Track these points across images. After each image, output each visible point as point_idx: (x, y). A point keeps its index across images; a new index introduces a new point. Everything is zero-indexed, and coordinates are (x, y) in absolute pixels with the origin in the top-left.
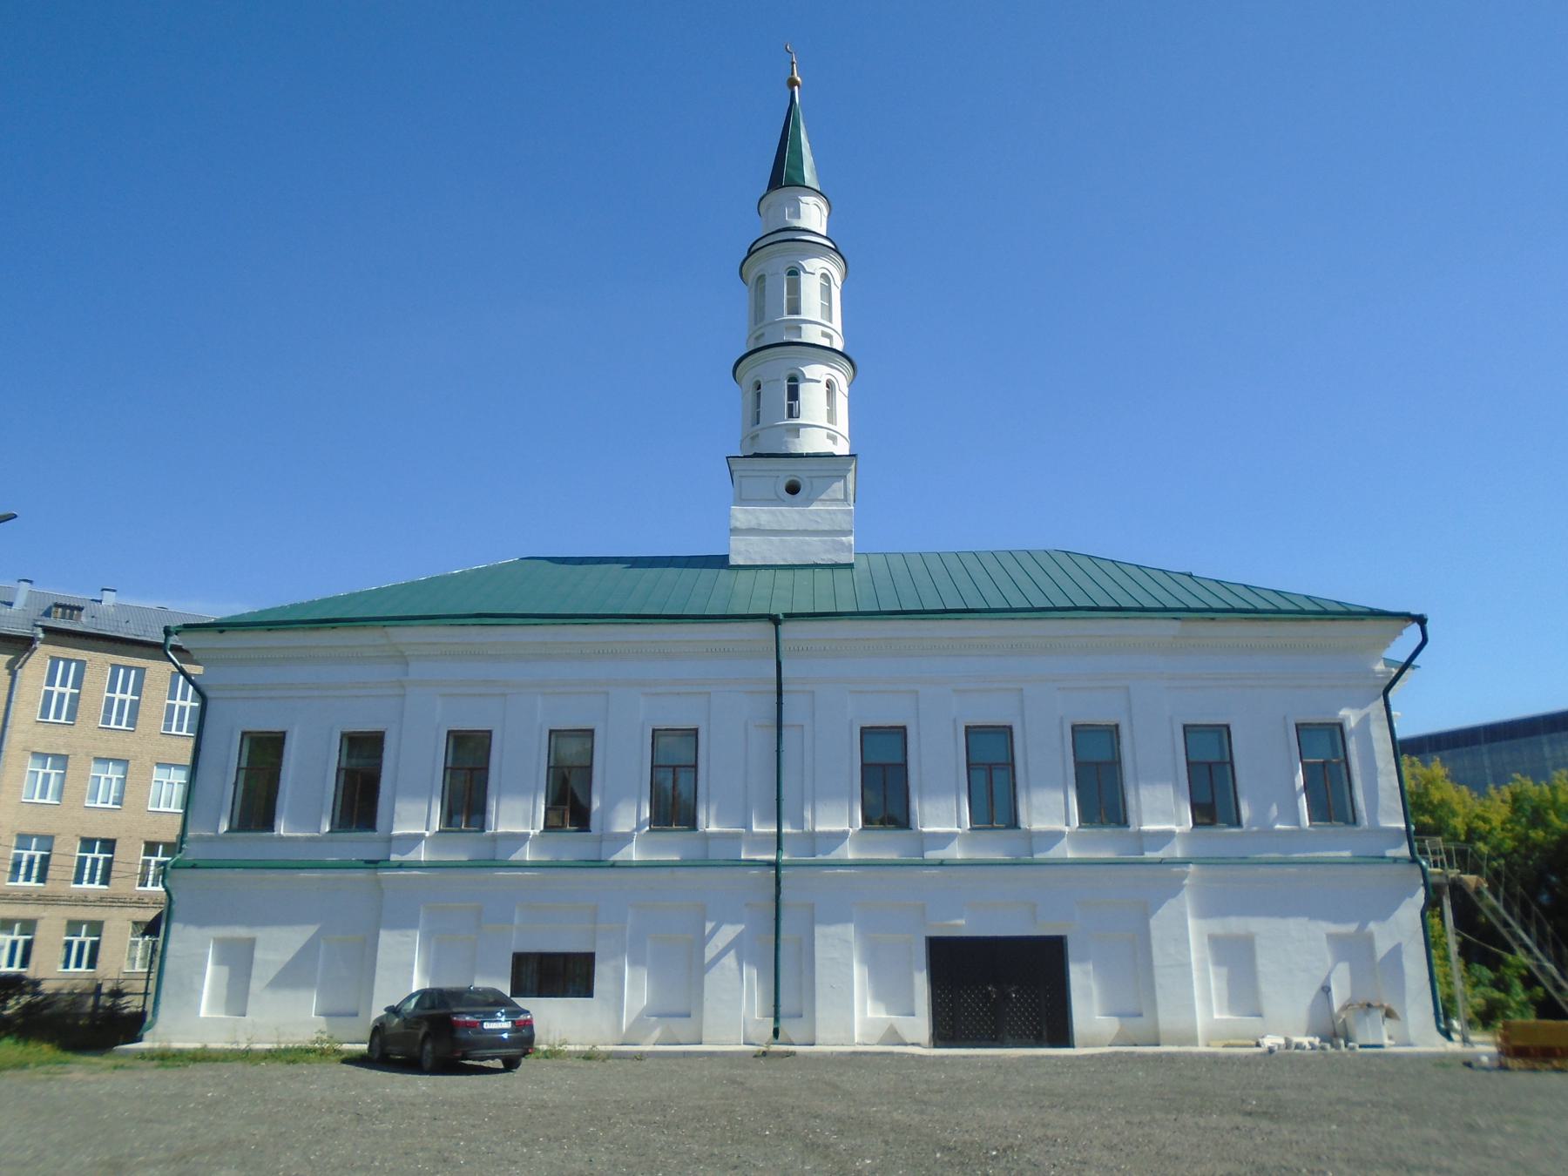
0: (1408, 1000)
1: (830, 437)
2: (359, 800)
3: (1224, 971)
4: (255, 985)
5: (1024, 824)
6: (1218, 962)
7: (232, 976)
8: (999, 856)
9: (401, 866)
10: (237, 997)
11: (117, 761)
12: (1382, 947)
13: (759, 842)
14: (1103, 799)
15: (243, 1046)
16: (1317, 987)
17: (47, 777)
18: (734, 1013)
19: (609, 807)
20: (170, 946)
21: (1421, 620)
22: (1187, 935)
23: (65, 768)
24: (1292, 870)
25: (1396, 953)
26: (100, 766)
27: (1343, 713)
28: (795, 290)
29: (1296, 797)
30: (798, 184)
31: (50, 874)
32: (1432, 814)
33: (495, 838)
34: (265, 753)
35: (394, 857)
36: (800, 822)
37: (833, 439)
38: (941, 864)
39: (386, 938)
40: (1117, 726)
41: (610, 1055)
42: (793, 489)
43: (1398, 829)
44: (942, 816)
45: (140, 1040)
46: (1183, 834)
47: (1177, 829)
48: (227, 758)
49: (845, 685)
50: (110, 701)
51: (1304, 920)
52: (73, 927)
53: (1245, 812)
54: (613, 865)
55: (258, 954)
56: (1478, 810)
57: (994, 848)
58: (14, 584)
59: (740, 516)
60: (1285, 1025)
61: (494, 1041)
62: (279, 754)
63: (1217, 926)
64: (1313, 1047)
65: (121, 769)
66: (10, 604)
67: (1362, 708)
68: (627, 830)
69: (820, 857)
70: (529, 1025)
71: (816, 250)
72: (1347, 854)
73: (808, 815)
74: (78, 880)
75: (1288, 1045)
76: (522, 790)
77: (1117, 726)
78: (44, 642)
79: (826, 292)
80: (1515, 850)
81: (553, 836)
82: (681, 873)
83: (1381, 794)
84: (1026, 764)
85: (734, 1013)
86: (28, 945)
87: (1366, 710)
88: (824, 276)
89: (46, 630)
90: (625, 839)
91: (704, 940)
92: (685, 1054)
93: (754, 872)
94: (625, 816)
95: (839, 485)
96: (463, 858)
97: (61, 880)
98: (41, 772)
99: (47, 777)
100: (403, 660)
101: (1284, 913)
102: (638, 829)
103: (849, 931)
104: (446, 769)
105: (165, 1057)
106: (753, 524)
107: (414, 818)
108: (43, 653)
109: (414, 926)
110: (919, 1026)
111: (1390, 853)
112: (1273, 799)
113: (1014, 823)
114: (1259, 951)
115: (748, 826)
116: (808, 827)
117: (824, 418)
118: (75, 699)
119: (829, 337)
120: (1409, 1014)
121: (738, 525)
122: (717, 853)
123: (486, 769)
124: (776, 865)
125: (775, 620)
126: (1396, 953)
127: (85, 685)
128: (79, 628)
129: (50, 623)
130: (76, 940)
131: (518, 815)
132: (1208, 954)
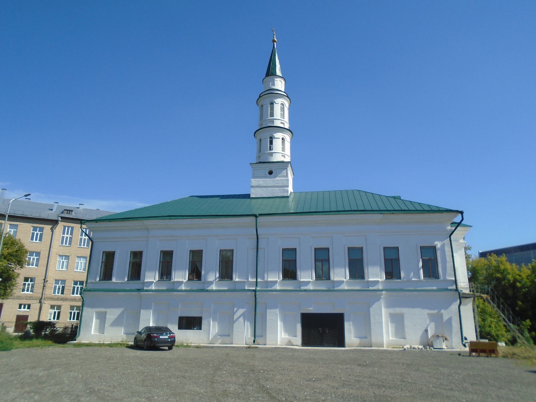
0: (453, 335)
1: (282, 156)
2: (136, 272)
3: (394, 325)
4: (107, 325)
5: (332, 278)
6: (392, 322)
7: (100, 322)
8: (324, 288)
9: (147, 291)
10: (101, 329)
11: (84, 257)
12: (445, 318)
13: (250, 284)
14: (357, 269)
15: (101, 342)
16: (424, 329)
17: (63, 262)
18: (243, 335)
19: (207, 274)
20: (83, 313)
21: (462, 213)
22: (382, 314)
23: (68, 260)
24: (416, 293)
25: (450, 319)
26: (79, 259)
27: (436, 243)
28: (272, 109)
29: (419, 270)
30: (274, 74)
31: (65, 292)
32: (501, 273)
33: (174, 282)
34: (109, 257)
35: (145, 288)
36: (263, 278)
37: (284, 156)
38: (305, 291)
39: (143, 312)
40: (362, 248)
41: (204, 347)
42: (271, 173)
43: (452, 280)
44: (307, 276)
45: (75, 340)
46: (382, 282)
47: (380, 280)
48: (99, 259)
49: (278, 237)
50: (63, 237)
51: (420, 309)
52: (72, 307)
53: (402, 275)
54: (207, 291)
55: (107, 316)
56: (518, 272)
57: (322, 286)
58: (53, 204)
59: (254, 182)
60: (413, 341)
61: (165, 341)
62: (113, 257)
63: (392, 311)
64: (419, 348)
65: (85, 260)
66: (52, 210)
67: (442, 241)
68: (212, 280)
69: (269, 288)
70: (174, 337)
71: (281, 96)
72: (435, 288)
73: (266, 276)
74: (73, 294)
75: (411, 348)
76: (181, 269)
77: (362, 248)
78: (61, 221)
79: (282, 109)
80: (531, 285)
81: (190, 282)
82: (227, 293)
83: (447, 269)
84: (333, 259)
85: (243, 335)
86: (59, 313)
87: (444, 242)
88: (282, 104)
89: (62, 218)
90: (211, 283)
91: (234, 313)
92: (226, 347)
93: (249, 293)
94: (211, 276)
95: (285, 171)
96: (165, 288)
97: (68, 293)
98: (62, 261)
99: (63, 262)
100: (147, 229)
101: (414, 307)
102: (215, 280)
103: (277, 311)
104: (160, 262)
105: (80, 345)
106: (258, 184)
107: (151, 277)
108: (61, 225)
109: (151, 309)
110: (298, 340)
111: (449, 288)
112: (412, 271)
113: (329, 278)
114: (405, 319)
115: (248, 279)
116: (266, 279)
117: (282, 149)
118: (71, 238)
119: (284, 124)
120: (453, 339)
121: (253, 185)
122: (238, 287)
123: (172, 262)
124: (255, 291)
125: (256, 216)
126: (450, 319)
127: (74, 234)
128: (71, 217)
129: (63, 215)
130: (73, 312)
131: (180, 276)
132: (389, 320)
